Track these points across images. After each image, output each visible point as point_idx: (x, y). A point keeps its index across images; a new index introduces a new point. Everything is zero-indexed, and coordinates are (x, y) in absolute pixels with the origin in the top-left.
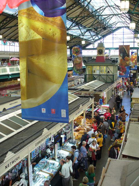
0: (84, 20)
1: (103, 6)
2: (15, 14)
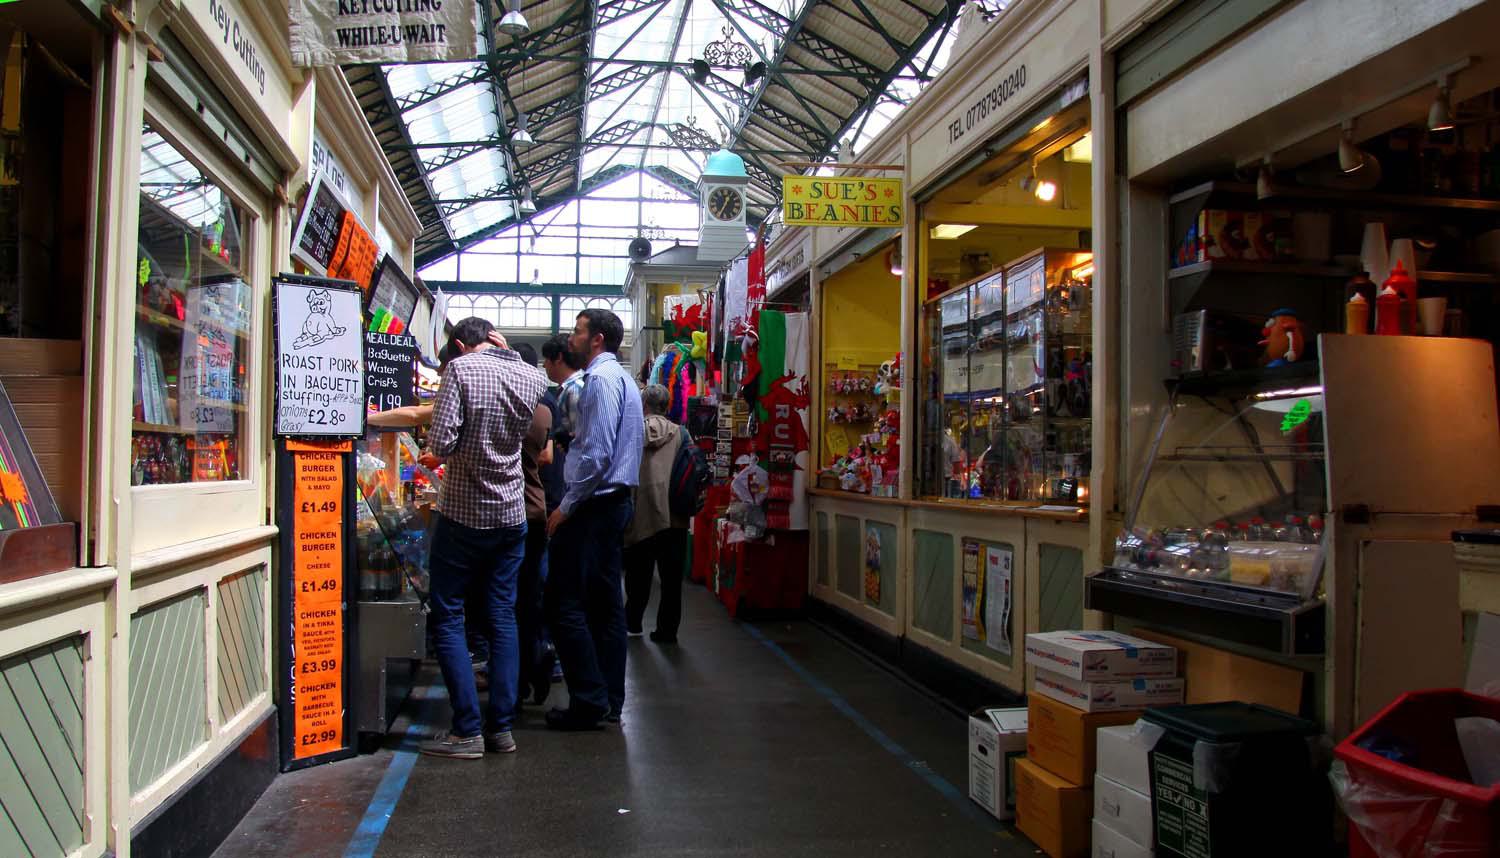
0: (784, 126)
1: (628, 122)
2: (406, 101)
